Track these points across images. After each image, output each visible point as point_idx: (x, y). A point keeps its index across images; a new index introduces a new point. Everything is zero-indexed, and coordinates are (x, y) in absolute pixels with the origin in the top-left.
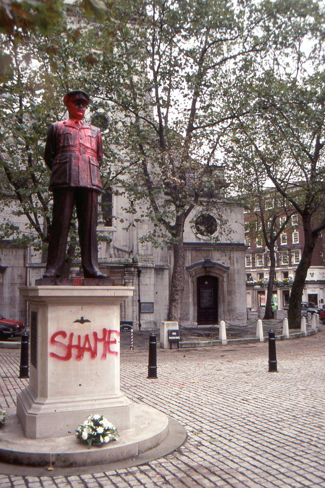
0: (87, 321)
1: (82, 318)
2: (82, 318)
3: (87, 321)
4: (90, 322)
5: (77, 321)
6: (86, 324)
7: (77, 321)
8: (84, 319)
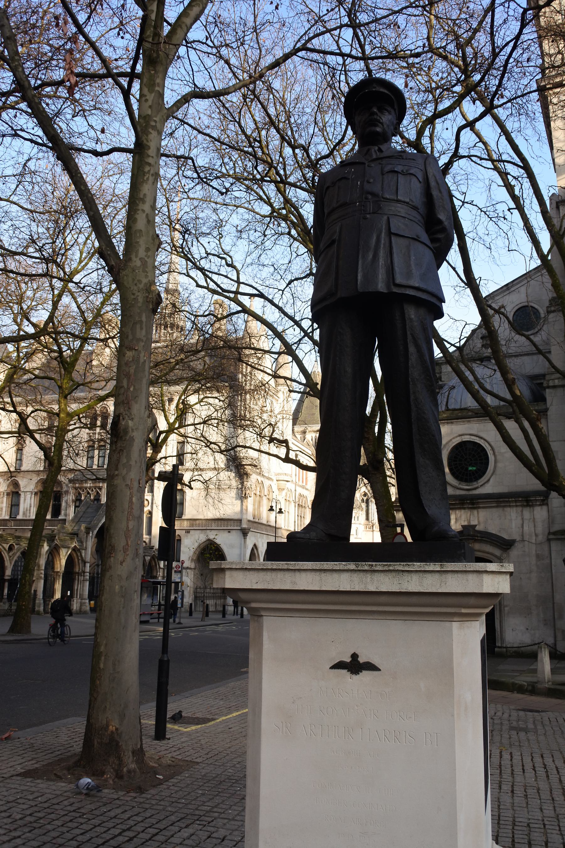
0: (371, 667)
1: (355, 656)
2: (355, 656)
3: (371, 667)
4: (380, 670)
5: (340, 666)
6: (365, 675)
7: (340, 666)
8: (361, 660)
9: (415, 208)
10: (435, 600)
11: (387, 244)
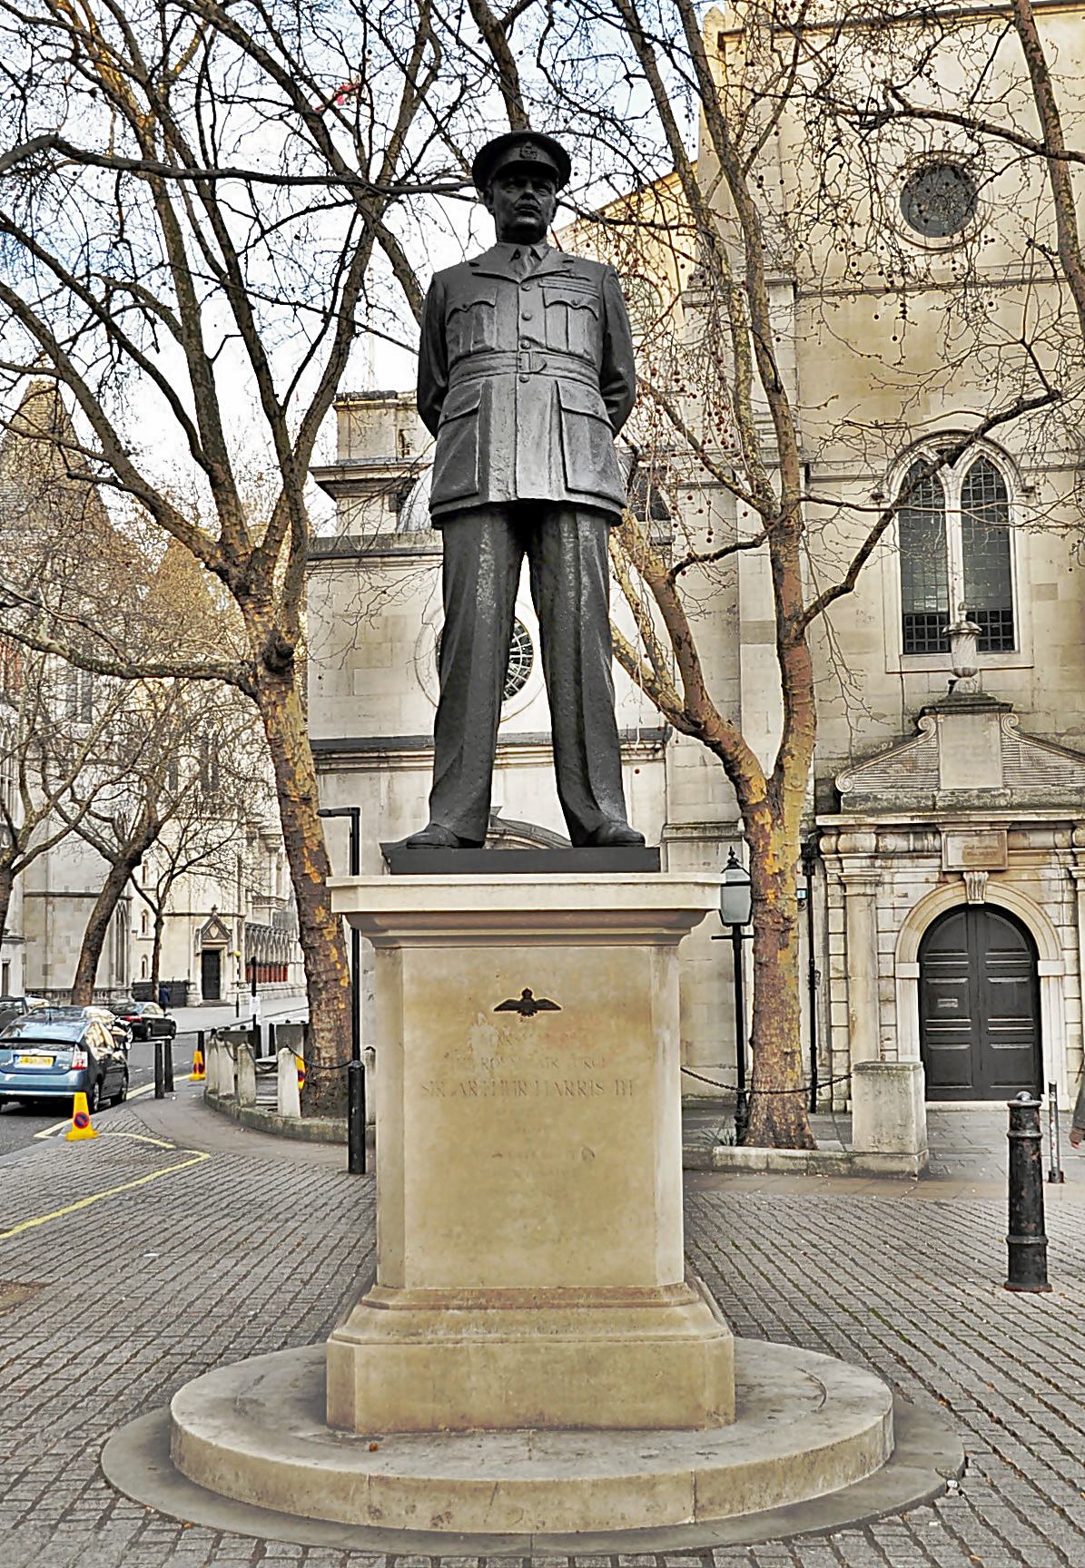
0: (547, 1005)
1: (527, 993)
2: (527, 993)
9: (590, 363)
10: (632, 918)
11: (555, 421)
